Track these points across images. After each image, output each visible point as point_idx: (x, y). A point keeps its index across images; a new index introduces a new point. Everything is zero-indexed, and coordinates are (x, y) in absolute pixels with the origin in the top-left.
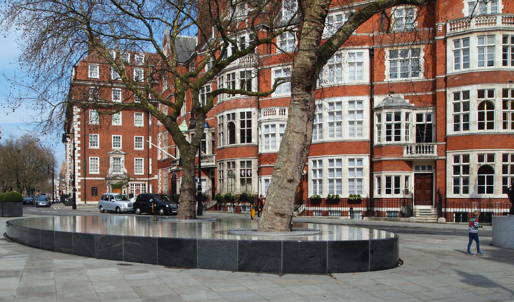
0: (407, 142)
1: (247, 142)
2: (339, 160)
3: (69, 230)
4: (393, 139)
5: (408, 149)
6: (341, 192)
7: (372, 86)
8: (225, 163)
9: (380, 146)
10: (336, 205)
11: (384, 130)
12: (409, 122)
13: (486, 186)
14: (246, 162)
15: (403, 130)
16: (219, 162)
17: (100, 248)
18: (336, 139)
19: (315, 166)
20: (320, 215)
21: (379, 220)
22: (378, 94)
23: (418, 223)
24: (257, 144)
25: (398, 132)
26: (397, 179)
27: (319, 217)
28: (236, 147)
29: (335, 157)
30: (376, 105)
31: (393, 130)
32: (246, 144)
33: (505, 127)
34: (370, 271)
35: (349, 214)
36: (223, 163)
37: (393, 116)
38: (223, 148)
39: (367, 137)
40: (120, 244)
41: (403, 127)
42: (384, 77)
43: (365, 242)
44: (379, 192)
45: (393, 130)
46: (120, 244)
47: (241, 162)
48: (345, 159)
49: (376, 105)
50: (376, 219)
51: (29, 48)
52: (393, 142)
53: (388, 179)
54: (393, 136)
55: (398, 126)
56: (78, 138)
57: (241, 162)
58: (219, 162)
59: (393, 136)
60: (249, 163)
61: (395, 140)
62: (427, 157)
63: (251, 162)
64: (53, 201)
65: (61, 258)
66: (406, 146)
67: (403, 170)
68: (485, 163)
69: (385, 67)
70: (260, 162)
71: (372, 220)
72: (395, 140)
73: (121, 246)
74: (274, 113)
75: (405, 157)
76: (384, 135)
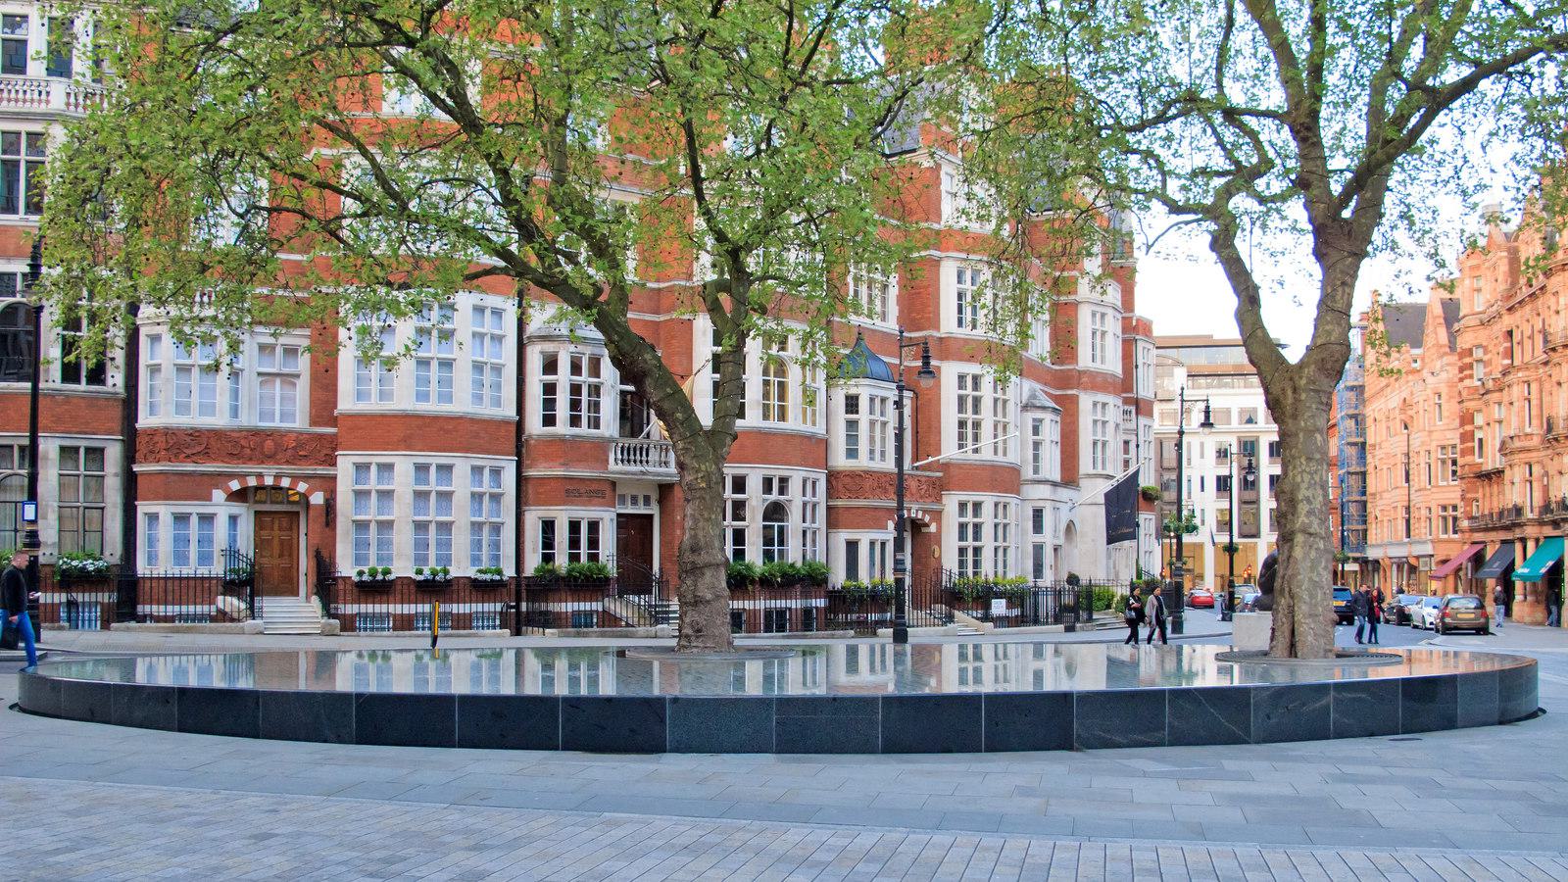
1: (88, 383)
2: (446, 469)
3: (508, 688)
6: (448, 559)
10: (385, 598)
14: (82, 451)
17: (1269, 718)
18: (432, 407)
19: (70, 464)
20: (494, 627)
21: (585, 635)
23: (448, 639)
27: (491, 631)
29: (435, 459)
32: (83, 386)
33: (766, 417)
34: (883, 752)
35: (63, 615)
39: (510, 411)
40: (1324, 702)
43: (507, 699)
46: (1324, 702)
47: (63, 449)
48: (462, 464)
49: (532, 328)
50: (578, 635)
52: (584, 430)
57: (63, 449)
60: (96, 454)
62: (659, 475)
63: (102, 450)
65: (918, 762)
68: (774, 496)
70: (130, 456)
71: (568, 635)
73: (1327, 707)
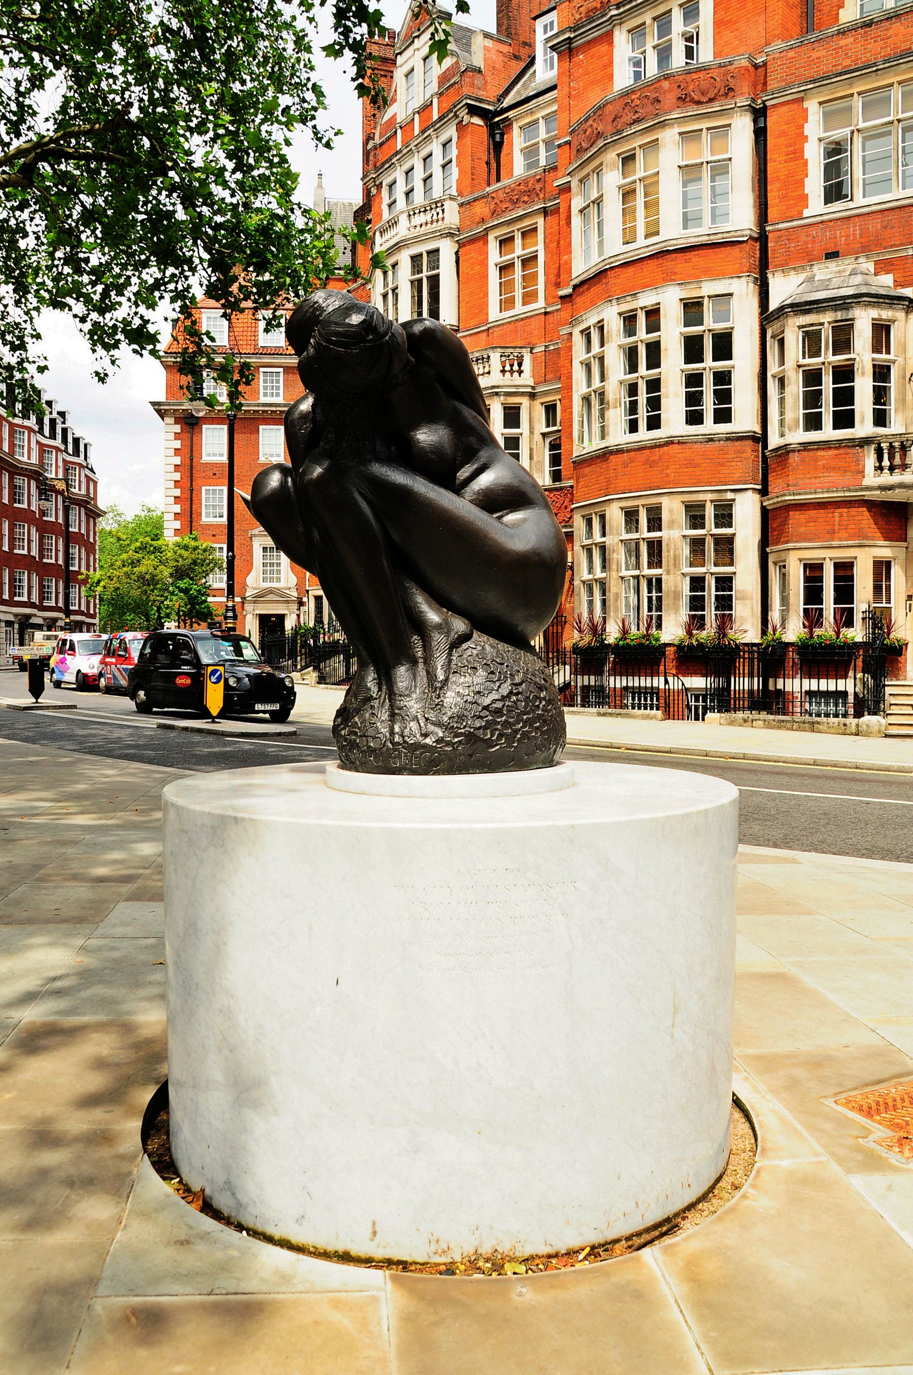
0: (881, 431)
4: (828, 420)
5: (880, 458)
7: (762, 239)
8: (615, 514)
9: (784, 452)
11: (796, 388)
12: (891, 357)
13: (884, 583)
15: (864, 387)
16: (586, 512)
22: (785, 267)
24: (757, 429)
25: (844, 397)
26: (844, 571)
28: (669, 443)
30: (773, 305)
31: (828, 386)
36: (603, 517)
37: (827, 335)
38: (605, 455)
41: (863, 374)
42: (803, 199)
44: (591, 569)
45: (828, 386)
49: (773, 305)
51: (267, 201)
53: (813, 572)
54: (827, 411)
55: (844, 374)
56: (175, 497)
58: (586, 512)
59: (827, 411)
61: (835, 427)
64: (114, 134)
66: (873, 446)
67: (862, 541)
69: (806, 163)
72: (835, 427)
74: (516, 368)
75: (868, 488)
76: (796, 411)
